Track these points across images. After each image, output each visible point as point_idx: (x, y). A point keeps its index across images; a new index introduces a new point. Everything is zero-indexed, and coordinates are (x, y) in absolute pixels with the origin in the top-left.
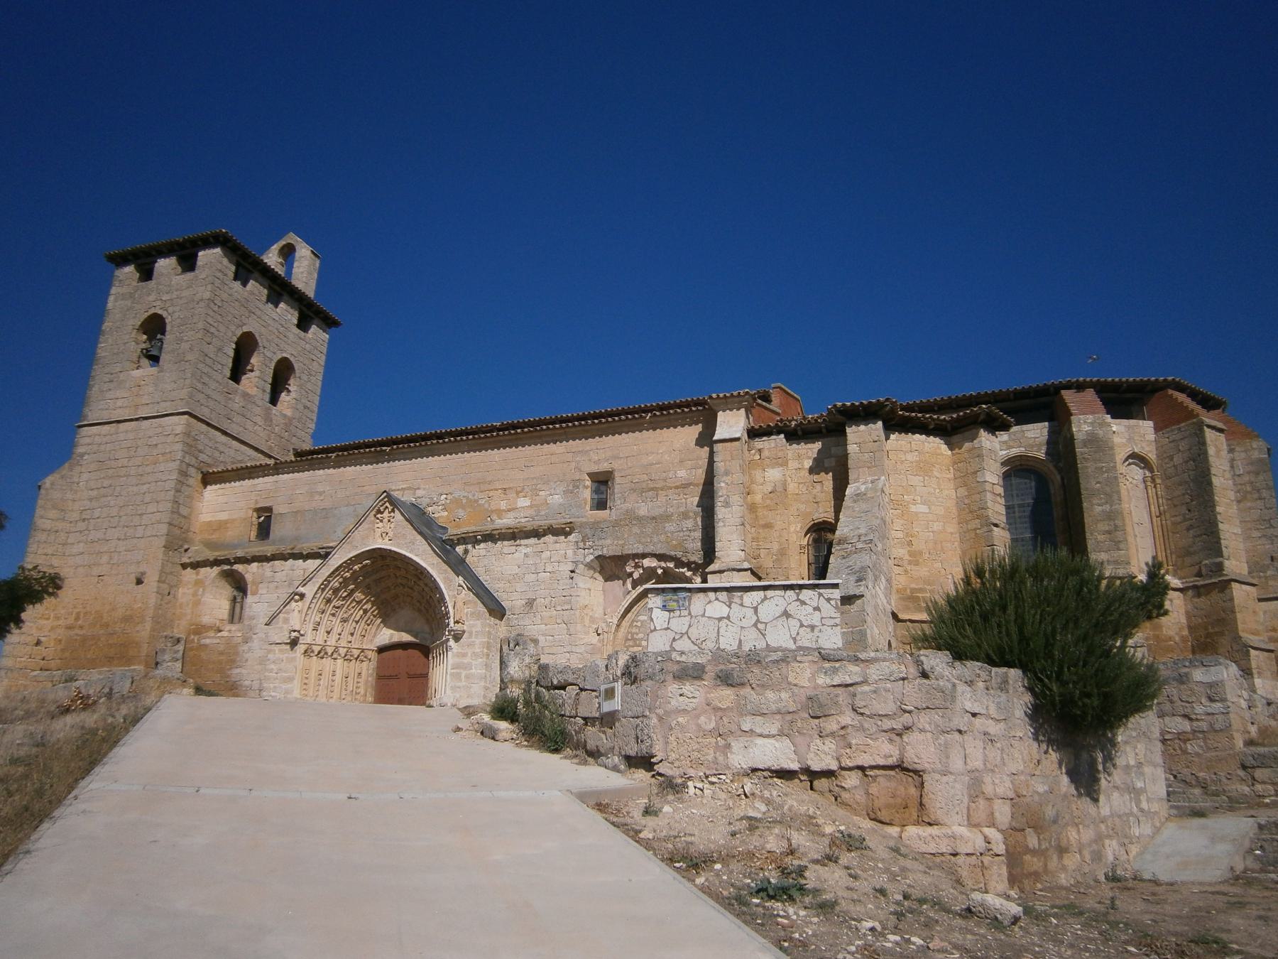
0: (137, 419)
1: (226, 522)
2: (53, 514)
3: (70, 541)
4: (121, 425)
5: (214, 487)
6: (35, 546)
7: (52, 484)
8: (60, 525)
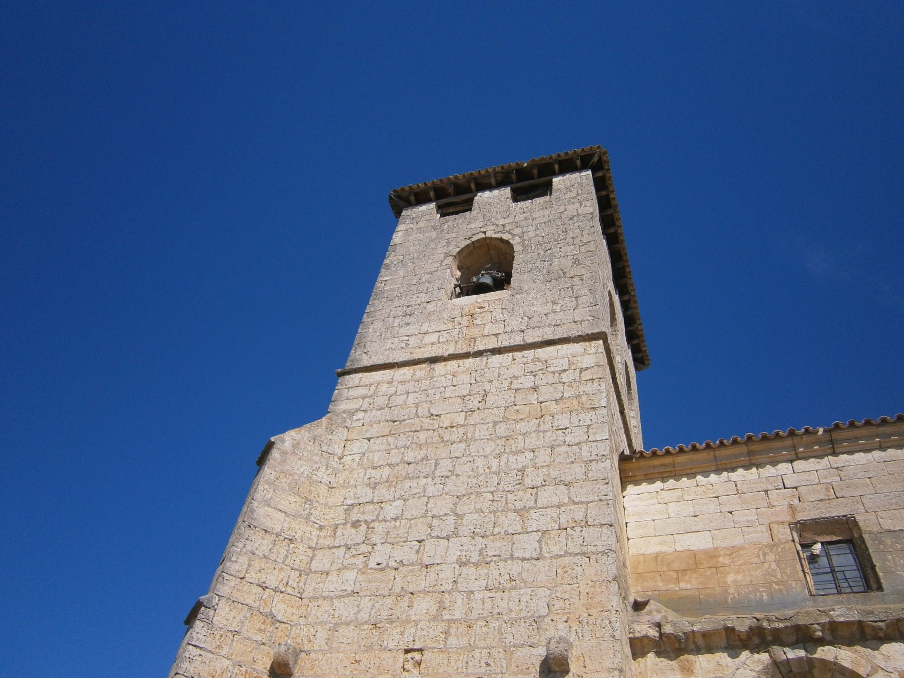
0: (479, 354)
1: (712, 555)
2: (290, 502)
3: (315, 565)
4: (439, 367)
5: (645, 487)
6: (244, 560)
7: (296, 445)
8: (299, 528)
